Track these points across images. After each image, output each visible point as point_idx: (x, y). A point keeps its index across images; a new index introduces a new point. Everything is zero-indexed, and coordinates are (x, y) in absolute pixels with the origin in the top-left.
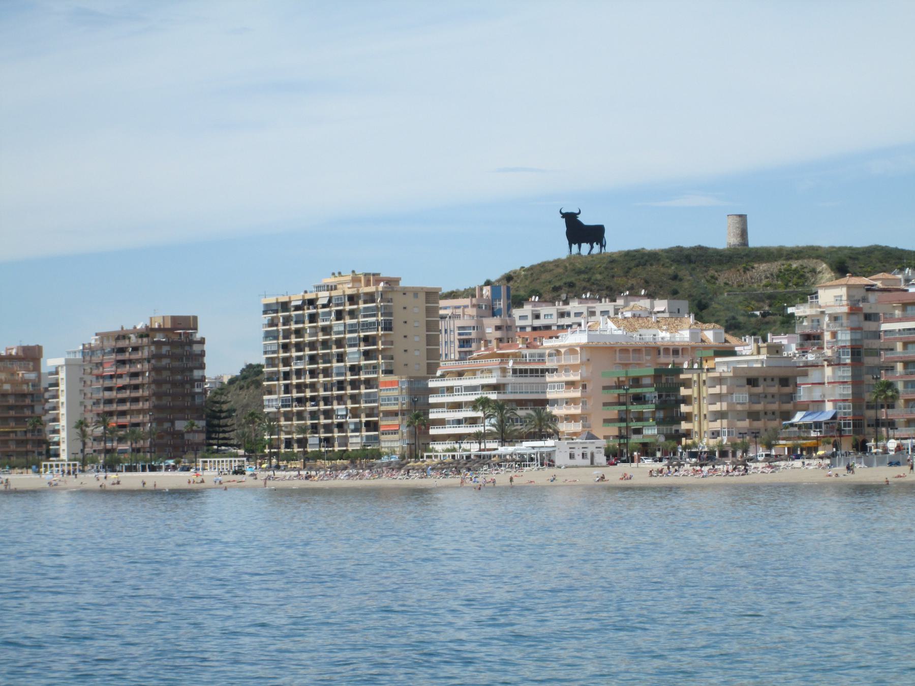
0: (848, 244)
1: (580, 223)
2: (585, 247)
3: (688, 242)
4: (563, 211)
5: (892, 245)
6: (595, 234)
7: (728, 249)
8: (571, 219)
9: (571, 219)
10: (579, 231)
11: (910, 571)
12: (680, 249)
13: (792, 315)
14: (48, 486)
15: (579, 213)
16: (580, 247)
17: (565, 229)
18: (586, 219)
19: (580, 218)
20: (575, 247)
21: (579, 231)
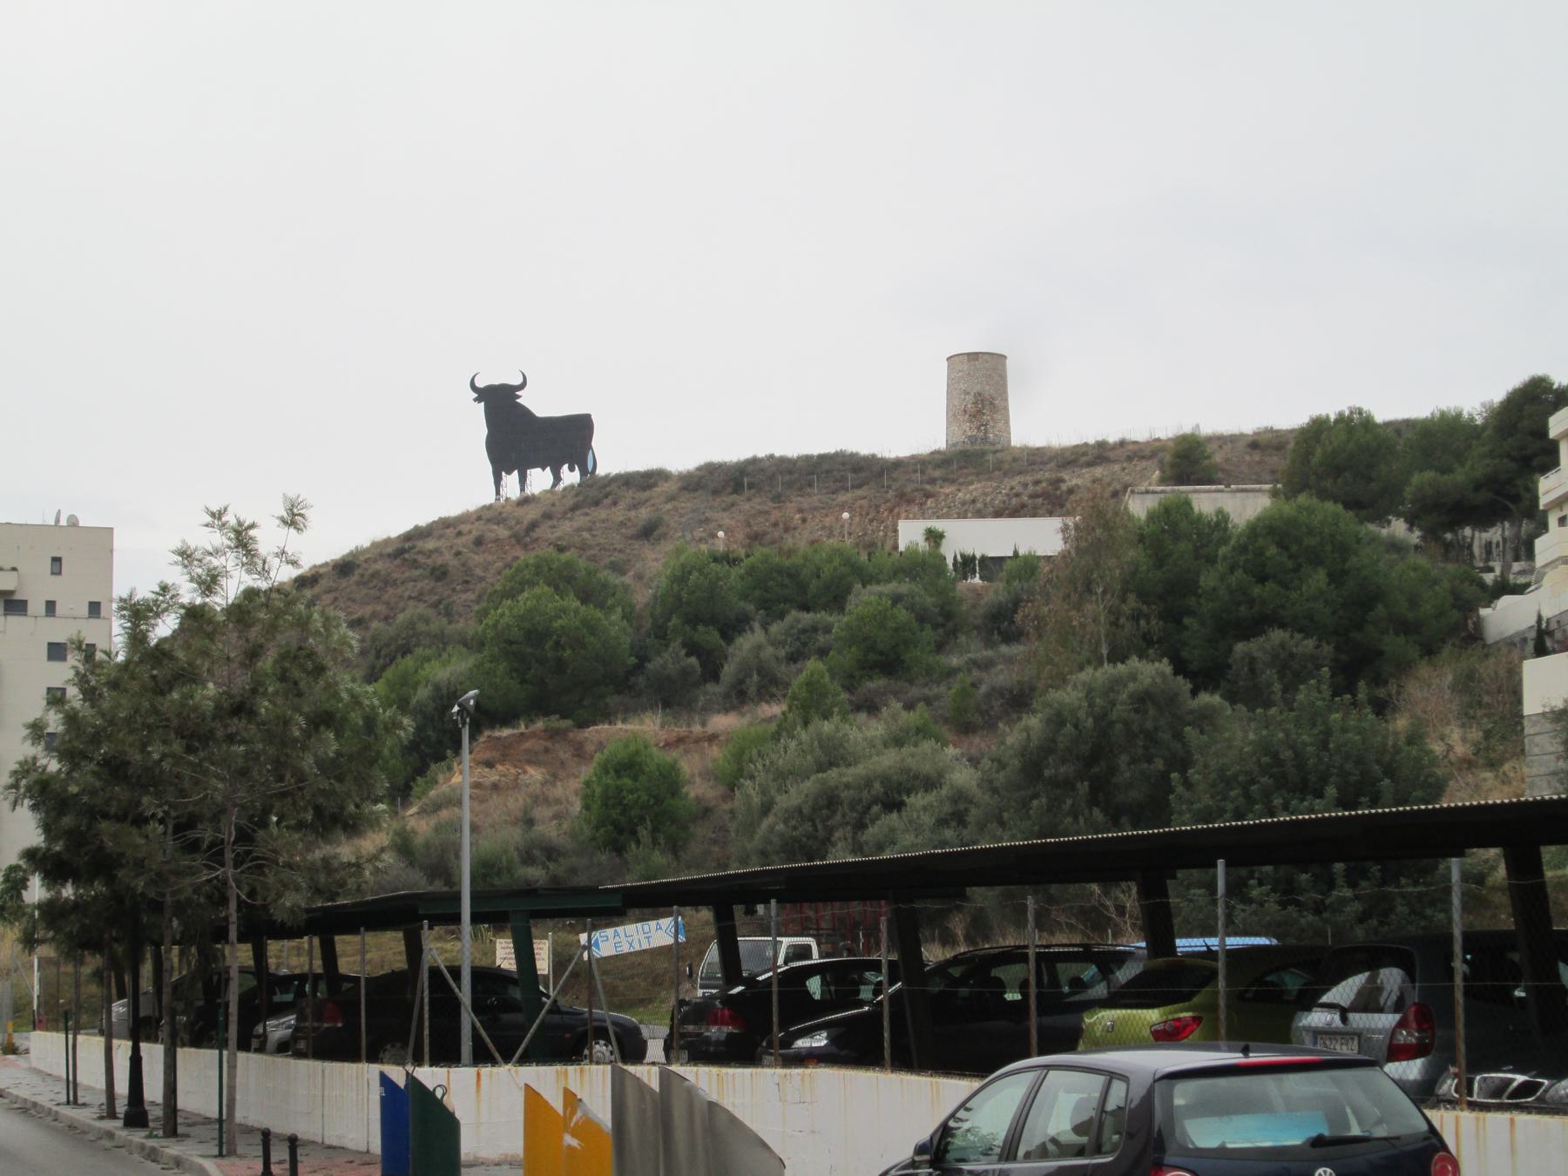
0: (380, 535)
1: (526, 413)
2: (540, 480)
3: (733, 452)
4: (480, 384)
5: (864, 450)
6: (569, 439)
7: (1148, 443)
8: (501, 404)
9: (501, 404)
10: (516, 432)
11: (1563, 866)
12: (1356, 427)
13: (1215, 866)
14: (19, 1040)
15: (522, 386)
16: (523, 480)
17: (485, 431)
18: (542, 402)
19: (526, 399)
20: (511, 481)
21: (516, 432)
